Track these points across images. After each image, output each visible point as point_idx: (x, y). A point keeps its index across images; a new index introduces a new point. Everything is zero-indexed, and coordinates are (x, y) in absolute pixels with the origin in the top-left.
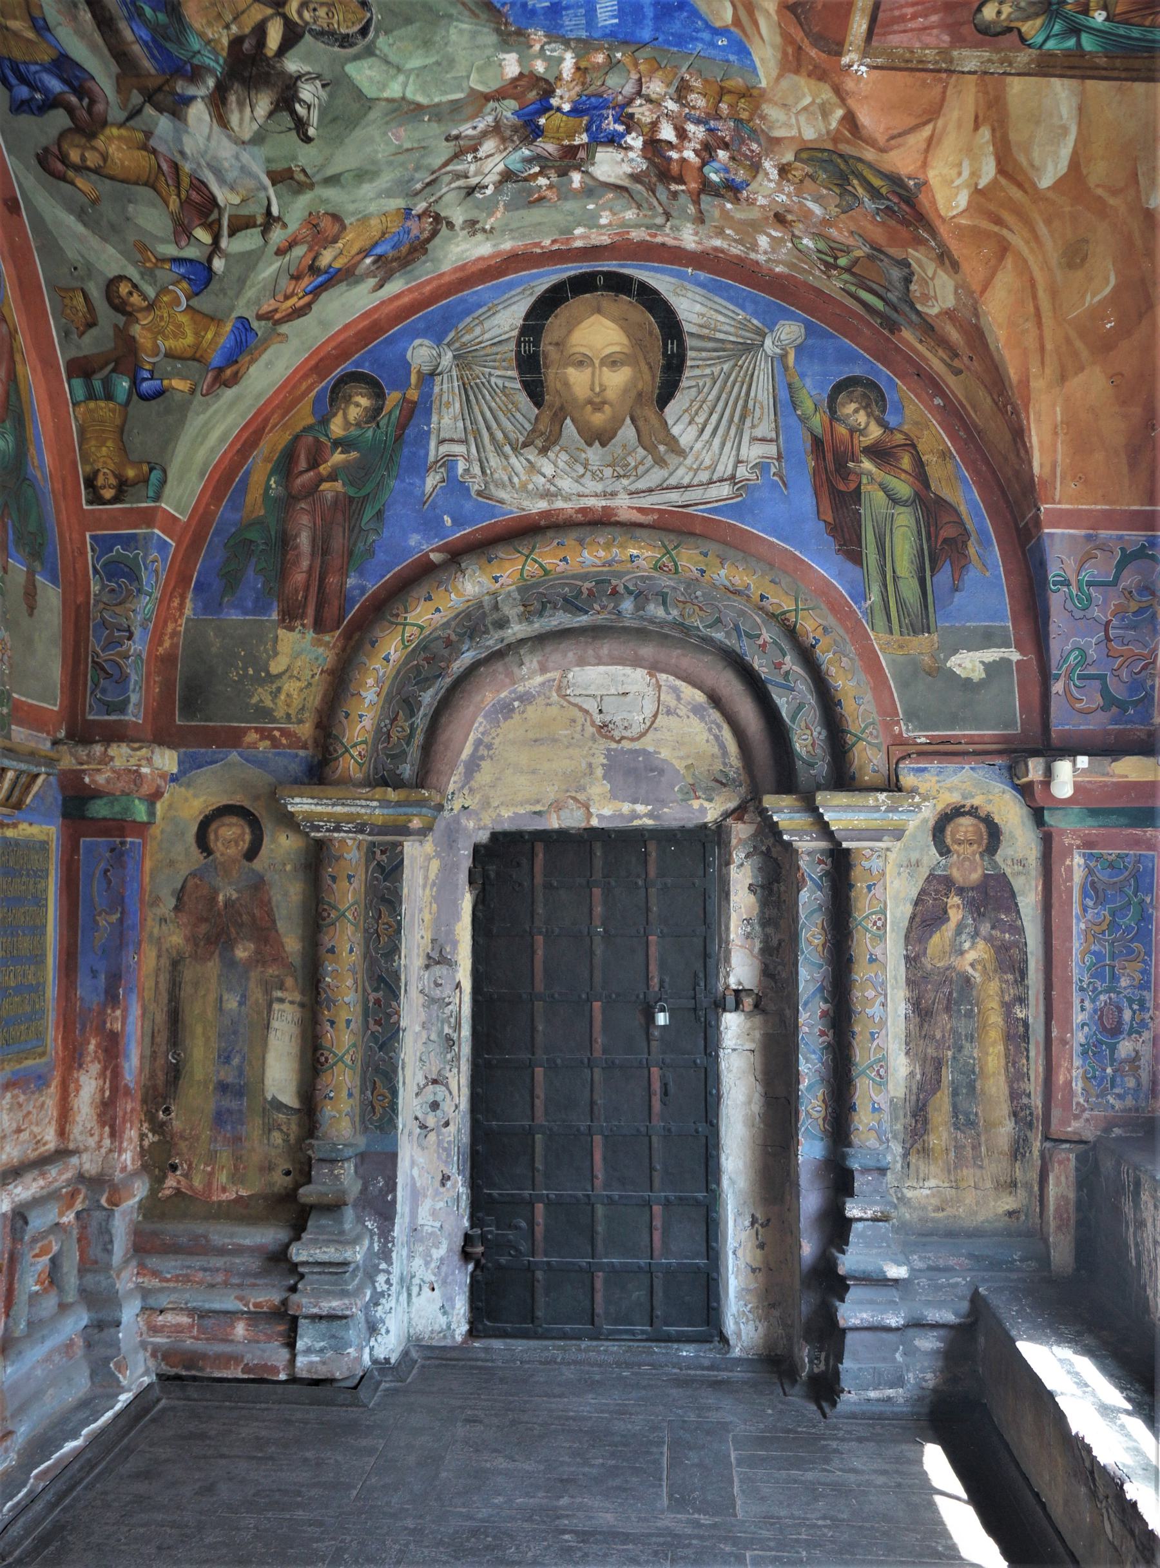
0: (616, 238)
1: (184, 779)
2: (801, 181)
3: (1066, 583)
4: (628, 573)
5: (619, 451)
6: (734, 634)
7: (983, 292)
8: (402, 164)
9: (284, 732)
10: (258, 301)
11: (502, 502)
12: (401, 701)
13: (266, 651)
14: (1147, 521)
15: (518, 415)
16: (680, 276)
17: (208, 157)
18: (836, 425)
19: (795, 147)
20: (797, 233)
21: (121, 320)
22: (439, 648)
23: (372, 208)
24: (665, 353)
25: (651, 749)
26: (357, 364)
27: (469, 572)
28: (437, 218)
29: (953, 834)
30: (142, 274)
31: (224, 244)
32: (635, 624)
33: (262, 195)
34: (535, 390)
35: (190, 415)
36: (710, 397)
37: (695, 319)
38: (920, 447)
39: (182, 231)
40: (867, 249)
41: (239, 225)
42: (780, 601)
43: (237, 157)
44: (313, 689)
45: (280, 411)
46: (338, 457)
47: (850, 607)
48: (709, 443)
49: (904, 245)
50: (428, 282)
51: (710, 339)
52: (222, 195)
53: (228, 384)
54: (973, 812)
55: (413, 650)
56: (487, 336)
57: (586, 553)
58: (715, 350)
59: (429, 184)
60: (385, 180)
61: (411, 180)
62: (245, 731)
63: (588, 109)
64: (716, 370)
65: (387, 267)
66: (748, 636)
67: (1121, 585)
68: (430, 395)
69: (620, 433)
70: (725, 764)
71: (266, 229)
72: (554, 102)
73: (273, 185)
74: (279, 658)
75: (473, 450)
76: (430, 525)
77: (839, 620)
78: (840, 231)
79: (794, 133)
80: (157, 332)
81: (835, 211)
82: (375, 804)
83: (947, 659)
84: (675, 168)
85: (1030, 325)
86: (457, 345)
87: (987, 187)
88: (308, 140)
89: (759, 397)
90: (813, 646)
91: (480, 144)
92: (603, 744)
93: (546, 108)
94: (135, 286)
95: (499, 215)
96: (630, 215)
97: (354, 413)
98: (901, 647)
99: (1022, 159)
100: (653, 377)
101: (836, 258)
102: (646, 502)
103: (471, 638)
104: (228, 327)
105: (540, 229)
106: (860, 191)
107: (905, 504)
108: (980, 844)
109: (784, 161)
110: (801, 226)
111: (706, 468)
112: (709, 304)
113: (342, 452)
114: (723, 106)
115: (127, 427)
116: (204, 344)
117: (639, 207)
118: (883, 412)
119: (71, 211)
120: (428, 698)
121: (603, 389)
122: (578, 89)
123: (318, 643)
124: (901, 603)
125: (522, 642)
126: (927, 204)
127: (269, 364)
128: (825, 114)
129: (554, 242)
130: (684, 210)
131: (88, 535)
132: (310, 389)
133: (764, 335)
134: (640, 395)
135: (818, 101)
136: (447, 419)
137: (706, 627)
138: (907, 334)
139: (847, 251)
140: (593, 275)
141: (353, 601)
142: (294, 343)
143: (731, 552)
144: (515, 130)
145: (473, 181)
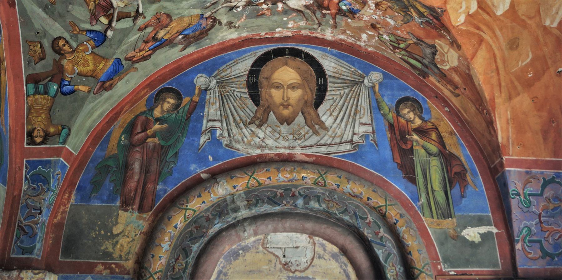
2: (386, 10)
3: (518, 194)
4: (301, 186)
6: (354, 216)
7: (472, 59)
10: (126, 52)
11: (238, 150)
12: (181, 248)
13: (112, 222)
14: (556, 165)
15: (247, 110)
20: (381, 33)
21: (58, 57)
22: (203, 222)
23: (186, 13)
25: (311, 277)
27: (221, 183)
28: (215, 20)
30: (71, 37)
31: (114, 24)
35: (87, 102)
36: (340, 104)
37: (331, 69)
38: (440, 130)
39: (94, 17)
40: (415, 40)
41: (122, 16)
42: (378, 201)
44: (135, 242)
45: (129, 104)
46: (157, 127)
47: (412, 204)
49: (434, 38)
50: (207, 48)
51: (339, 78)
53: (107, 89)
55: (189, 223)
56: (233, 74)
57: (280, 175)
59: (213, 4)
62: (96, 265)
64: (342, 92)
65: (188, 41)
66: (361, 218)
67: (545, 196)
68: (205, 99)
69: (296, 119)
71: (135, 18)
74: (118, 225)
75: (225, 125)
78: (402, 31)
80: (75, 63)
81: (400, 23)
83: (461, 231)
85: (494, 74)
86: (219, 77)
89: (363, 105)
90: (395, 224)
92: (285, 274)
94: (67, 42)
95: (242, 20)
96: (302, 23)
97: (166, 106)
98: (438, 225)
100: (312, 94)
101: (399, 44)
102: (309, 151)
104: (111, 62)
105: (261, 28)
106: (414, 14)
107: (435, 155)
110: (383, 30)
111: (339, 136)
113: (159, 124)
116: (98, 70)
117: (307, 20)
118: (422, 113)
119: (40, 7)
120: (196, 248)
123: (140, 218)
124: (436, 203)
125: (245, 219)
126: (446, 20)
127: (128, 81)
129: (266, 34)
130: (327, 22)
131: (25, 160)
132: (145, 94)
133: (364, 78)
134: (306, 102)
136: (212, 110)
137: (340, 213)
138: (432, 79)
139: (405, 40)
140: (284, 49)
142: (140, 72)
143: (352, 176)
145: (233, 4)
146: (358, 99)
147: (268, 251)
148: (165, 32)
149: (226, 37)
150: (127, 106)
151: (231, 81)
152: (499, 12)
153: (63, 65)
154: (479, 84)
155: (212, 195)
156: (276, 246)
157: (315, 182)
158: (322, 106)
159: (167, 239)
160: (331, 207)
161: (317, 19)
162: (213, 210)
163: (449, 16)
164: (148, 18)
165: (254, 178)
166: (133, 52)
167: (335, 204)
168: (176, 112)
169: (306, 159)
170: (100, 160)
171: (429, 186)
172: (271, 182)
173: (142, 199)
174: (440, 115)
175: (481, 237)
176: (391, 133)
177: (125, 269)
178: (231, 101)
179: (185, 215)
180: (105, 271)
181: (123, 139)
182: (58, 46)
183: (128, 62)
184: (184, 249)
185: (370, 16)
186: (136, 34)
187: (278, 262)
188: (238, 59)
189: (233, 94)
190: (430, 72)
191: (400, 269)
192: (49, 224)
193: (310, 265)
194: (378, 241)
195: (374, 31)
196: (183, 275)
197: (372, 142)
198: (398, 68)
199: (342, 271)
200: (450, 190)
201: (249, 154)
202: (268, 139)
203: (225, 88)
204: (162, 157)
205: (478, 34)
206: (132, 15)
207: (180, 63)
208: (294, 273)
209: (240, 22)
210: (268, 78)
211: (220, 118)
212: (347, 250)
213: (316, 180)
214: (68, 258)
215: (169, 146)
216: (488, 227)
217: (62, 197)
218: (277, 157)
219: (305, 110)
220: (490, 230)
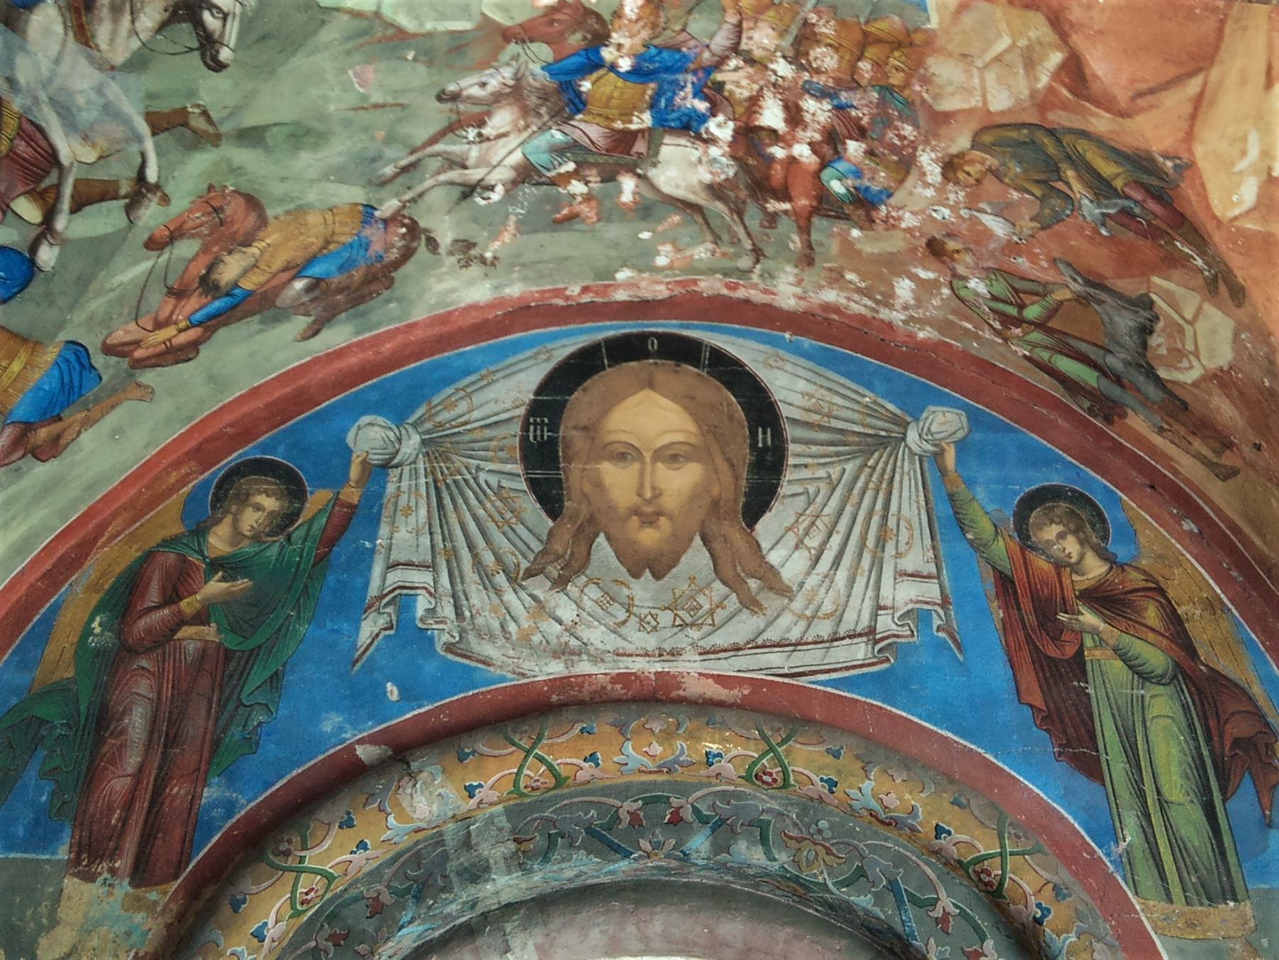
0: (678, 290)
2: (978, 181)
8: (366, 129)
10: (107, 321)
13: (35, 917)
15: (520, 529)
17: (51, 91)
18: (1031, 556)
19: (974, 126)
20: (961, 270)
22: (357, 917)
23: (312, 196)
26: (265, 448)
27: (424, 775)
28: (414, 229)
31: (60, 224)
32: (710, 879)
33: (134, 149)
34: (550, 496)
36: (827, 510)
37: (798, 400)
38: (1171, 594)
42: (973, 838)
43: (100, 90)
45: (126, 515)
46: (215, 587)
47: (1093, 852)
48: (829, 577)
49: (1146, 270)
51: (822, 428)
52: (67, 147)
56: (476, 415)
59: (405, 170)
60: (338, 149)
61: (377, 158)
63: (655, 72)
68: (380, 496)
69: (683, 559)
71: (134, 201)
72: (607, 54)
73: (154, 134)
74: (59, 930)
75: (444, 579)
76: (360, 695)
77: (1076, 874)
78: (1033, 259)
79: (975, 101)
81: (1028, 225)
84: (777, 173)
86: (429, 425)
88: (217, 66)
89: (905, 511)
90: (1039, 922)
91: (489, 114)
93: (594, 65)
95: (507, 237)
96: (701, 252)
97: (250, 519)
98: (1191, 925)
100: (736, 478)
101: (1021, 307)
102: (728, 666)
103: (419, 899)
104: (50, 355)
107: (1160, 680)
109: (954, 150)
110: (968, 258)
111: (827, 616)
112: (819, 380)
113: (223, 579)
114: (865, 66)
117: (717, 239)
118: (1105, 538)
121: (658, 494)
122: (645, 34)
123: (135, 904)
124: (1178, 847)
126: (1194, 198)
127: (117, 431)
128: (1031, 62)
129: (585, 290)
132: (182, 482)
133: (905, 425)
134: (716, 503)
135: (1022, 43)
136: (404, 531)
137: (840, 884)
138: (1138, 422)
139: (1041, 291)
140: (643, 337)
142: (164, 406)
144: (544, 96)
145: (474, 175)
146: (889, 494)
148: (244, 264)
149: (455, 295)
150: (119, 520)
151: (467, 438)
155: (391, 819)
158: (768, 515)
163: (1203, 185)
164: (180, 204)
165: (541, 759)
166: (132, 326)
167: (822, 851)
168: (281, 538)
170: (14, 701)
171: (1148, 787)
172: (596, 772)
174: (1169, 546)
178: (466, 502)
179: (293, 892)
181: (98, 630)
185: (923, 211)
186: (136, 262)
189: (476, 479)
190: (1128, 398)
195: (940, 266)
197: (942, 634)
198: (1016, 396)
200: (1224, 801)
201: (523, 675)
202: (589, 626)
203: (448, 459)
204: (227, 691)
206: (123, 192)
207: (303, 382)
209: (497, 244)
210: (589, 429)
211: (429, 558)
213: (754, 764)
215: (253, 654)
218: (618, 686)
219: (713, 528)
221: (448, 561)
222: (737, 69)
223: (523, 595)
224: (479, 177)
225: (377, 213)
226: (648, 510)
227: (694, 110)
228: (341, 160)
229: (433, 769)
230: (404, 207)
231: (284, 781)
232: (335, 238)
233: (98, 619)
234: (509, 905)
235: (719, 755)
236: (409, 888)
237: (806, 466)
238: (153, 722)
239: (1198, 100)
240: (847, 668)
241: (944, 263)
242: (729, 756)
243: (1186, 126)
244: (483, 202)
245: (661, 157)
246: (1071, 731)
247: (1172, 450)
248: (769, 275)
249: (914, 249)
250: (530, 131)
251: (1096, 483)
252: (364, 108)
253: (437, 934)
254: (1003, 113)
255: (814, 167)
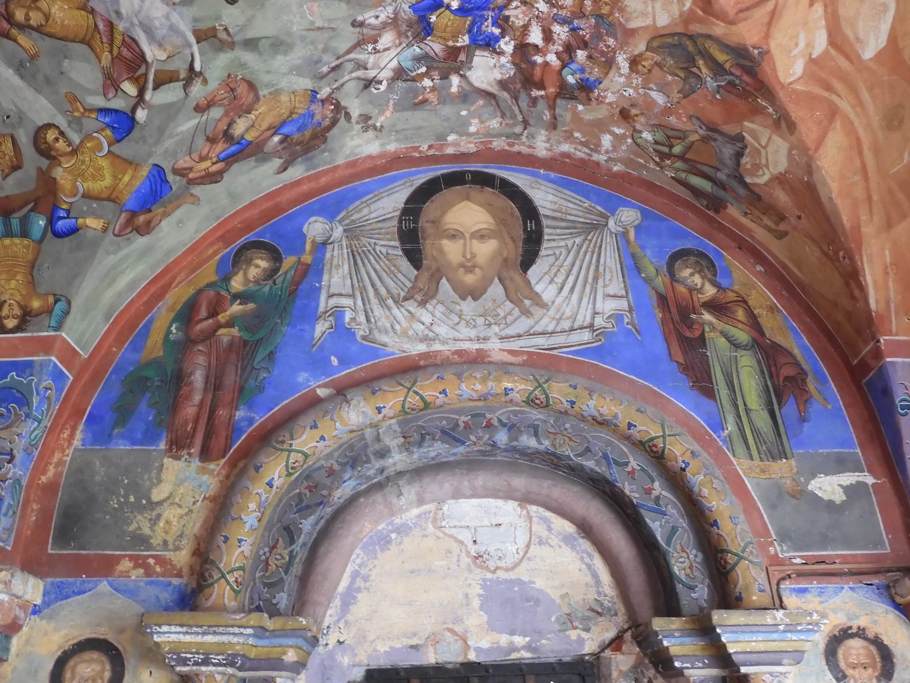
0: (481, 147)
1: (46, 611)
2: (650, 71)
5: (490, 304)
6: (604, 462)
8: (313, 43)
9: (159, 560)
13: (150, 479)
15: (400, 276)
16: (534, 175)
18: (676, 285)
19: (647, 36)
20: (638, 127)
21: (44, 163)
22: (321, 477)
23: (283, 84)
24: (525, 229)
26: (259, 234)
27: (353, 402)
28: (338, 107)
29: (846, 658)
30: (69, 123)
31: (148, 96)
33: (187, 51)
34: (415, 257)
36: (566, 263)
38: (750, 303)
39: (111, 83)
44: (194, 516)
46: (236, 308)
47: (710, 436)
48: (568, 298)
51: (562, 220)
52: (151, 52)
54: (861, 633)
56: (373, 215)
57: (463, 386)
58: (567, 228)
59: (334, 69)
63: (472, 9)
64: (570, 243)
66: (617, 463)
68: (323, 259)
69: (489, 290)
70: (599, 593)
73: (198, 43)
74: (162, 485)
75: (360, 302)
76: (318, 364)
77: (702, 447)
78: (679, 118)
79: (649, 22)
81: (676, 96)
82: (249, 631)
83: (807, 483)
84: (538, 71)
85: (858, 178)
86: (347, 221)
87: (819, 57)
90: (683, 470)
91: (380, 36)
92: (478, 574)
94: (62, 133)
95: (388, 114)
96: (494, 123)
97: (253, 272)
98: (763, 471)
99: (849, 32)
100: (516, 247)
101: (671, 147)
102: (515, 345)
103: (353, 467)
104: (145, 172)
107: (745, 347)
108: (874, 668)
109: (636, 52)
110: (642, 119)
111: (568, 318)
113: (240, 304)
115: (37, 263)
116: (121, 186)
117: (503, 115)
118: (715, 275)
119: (10, 64)
120: (308, 525)
121: (474, 256)
123: (203, 471)
124: (756, 432)
125: (400, 474)
126: (769, 71)
129: (430, 147)
132: (215, 253)
133: (607, 218)
134: (506, 260)
136: (336, 277)
139: (682, 136)
141: (241, 431)
142: (205, 209)
145: (371, 74)
146: (599, 254)
147: (445, 533)
148: (247, 124)
150: (183, 275)
151: (368, 228)
152: (868, 53)
153: (55, 179)
154: (831, 199)
155: (338, 424)
156: (457, 524)
157: (528, 397)
158: (534, 266)
159: (252, 506)
160: (561, 446)
161: (521, 111)
162: (340, 456)
163: (774, 64)
164: (213, 84)
165: (417, 393)
166: (188, 158)
167: (567, 439)
168: (271, 282)
169: (512, 359)
170: (132, 368)
173: (208, 436)
175: (845, 492)
176: (663, 311)
177: (174, 566)
178: (369, 261)
180: (134, 572)
181: (174, 331)
182: (46, 143)
183: (178, 178)
184: (287, 529)
185: (619, 91)
186: (190, 119)
187: (463, 554)
188: (381, 191)
191: (696, 556)
192: (29, 486)
193: (524, 557)
194: (651, 504)
196: (285, 577)
197: (629, 327)
199: (584, 566)
200: (780, 409)
201: (405, 352)
202: (439, 325)
205: (827, 99)
206: (181, 77)
208: (494, 572)
211: (350, 292)
212: (591, 527)
213: (530, 394)
214: (65, 549)
216: (857, 474)
217: (59, 435)
219: (505, 274)
220: (861, 479)
221: (361, 293)
222: (516, 8)
223: (403, 310)
224: (374, 75)
225: (318, 96)
226: (469, 264)
227: (492, 34)
228: (300, 61)
229: (358, 398)
230: (333, 92)
231: (279, 407)
232: (296, 110)
233: (174, 326)
234: (400, 472)
235: (512, 389)
236: (348, 462)
237: (554, 240)
238: (207, 377)
239: (773, 15)
240: (579, 345)
241: (629, 123)
242: (517, 389)
243: (765, 29)
244: (376, 91)
245: (474, 64)
246: (698, 375)
247: (752, 226)
248: (532, 136)
249: (613, 116)
250: (402, 47)
251: (710, 246)
252: (312, 30)
253: (363, 487)
254: (664, 27)
255: (558, 68)
